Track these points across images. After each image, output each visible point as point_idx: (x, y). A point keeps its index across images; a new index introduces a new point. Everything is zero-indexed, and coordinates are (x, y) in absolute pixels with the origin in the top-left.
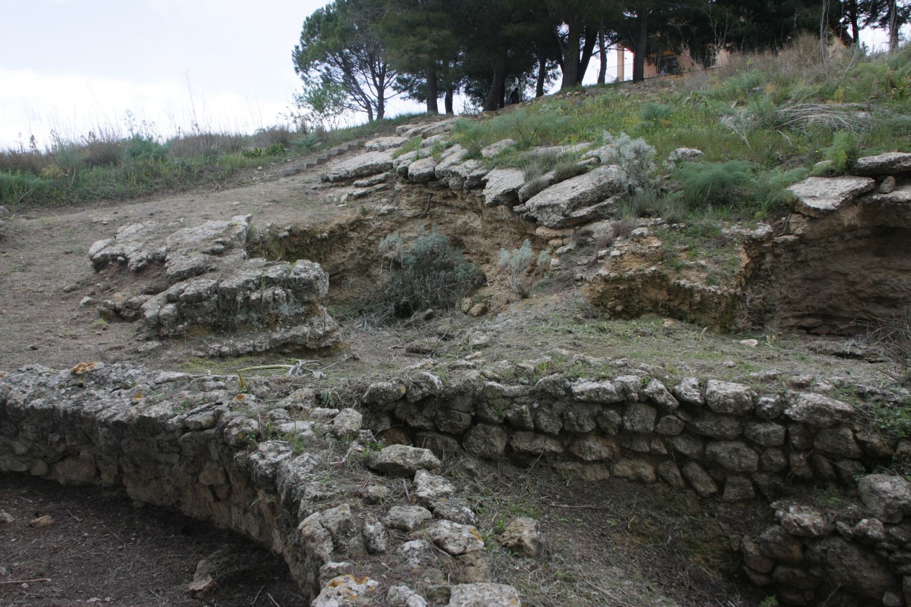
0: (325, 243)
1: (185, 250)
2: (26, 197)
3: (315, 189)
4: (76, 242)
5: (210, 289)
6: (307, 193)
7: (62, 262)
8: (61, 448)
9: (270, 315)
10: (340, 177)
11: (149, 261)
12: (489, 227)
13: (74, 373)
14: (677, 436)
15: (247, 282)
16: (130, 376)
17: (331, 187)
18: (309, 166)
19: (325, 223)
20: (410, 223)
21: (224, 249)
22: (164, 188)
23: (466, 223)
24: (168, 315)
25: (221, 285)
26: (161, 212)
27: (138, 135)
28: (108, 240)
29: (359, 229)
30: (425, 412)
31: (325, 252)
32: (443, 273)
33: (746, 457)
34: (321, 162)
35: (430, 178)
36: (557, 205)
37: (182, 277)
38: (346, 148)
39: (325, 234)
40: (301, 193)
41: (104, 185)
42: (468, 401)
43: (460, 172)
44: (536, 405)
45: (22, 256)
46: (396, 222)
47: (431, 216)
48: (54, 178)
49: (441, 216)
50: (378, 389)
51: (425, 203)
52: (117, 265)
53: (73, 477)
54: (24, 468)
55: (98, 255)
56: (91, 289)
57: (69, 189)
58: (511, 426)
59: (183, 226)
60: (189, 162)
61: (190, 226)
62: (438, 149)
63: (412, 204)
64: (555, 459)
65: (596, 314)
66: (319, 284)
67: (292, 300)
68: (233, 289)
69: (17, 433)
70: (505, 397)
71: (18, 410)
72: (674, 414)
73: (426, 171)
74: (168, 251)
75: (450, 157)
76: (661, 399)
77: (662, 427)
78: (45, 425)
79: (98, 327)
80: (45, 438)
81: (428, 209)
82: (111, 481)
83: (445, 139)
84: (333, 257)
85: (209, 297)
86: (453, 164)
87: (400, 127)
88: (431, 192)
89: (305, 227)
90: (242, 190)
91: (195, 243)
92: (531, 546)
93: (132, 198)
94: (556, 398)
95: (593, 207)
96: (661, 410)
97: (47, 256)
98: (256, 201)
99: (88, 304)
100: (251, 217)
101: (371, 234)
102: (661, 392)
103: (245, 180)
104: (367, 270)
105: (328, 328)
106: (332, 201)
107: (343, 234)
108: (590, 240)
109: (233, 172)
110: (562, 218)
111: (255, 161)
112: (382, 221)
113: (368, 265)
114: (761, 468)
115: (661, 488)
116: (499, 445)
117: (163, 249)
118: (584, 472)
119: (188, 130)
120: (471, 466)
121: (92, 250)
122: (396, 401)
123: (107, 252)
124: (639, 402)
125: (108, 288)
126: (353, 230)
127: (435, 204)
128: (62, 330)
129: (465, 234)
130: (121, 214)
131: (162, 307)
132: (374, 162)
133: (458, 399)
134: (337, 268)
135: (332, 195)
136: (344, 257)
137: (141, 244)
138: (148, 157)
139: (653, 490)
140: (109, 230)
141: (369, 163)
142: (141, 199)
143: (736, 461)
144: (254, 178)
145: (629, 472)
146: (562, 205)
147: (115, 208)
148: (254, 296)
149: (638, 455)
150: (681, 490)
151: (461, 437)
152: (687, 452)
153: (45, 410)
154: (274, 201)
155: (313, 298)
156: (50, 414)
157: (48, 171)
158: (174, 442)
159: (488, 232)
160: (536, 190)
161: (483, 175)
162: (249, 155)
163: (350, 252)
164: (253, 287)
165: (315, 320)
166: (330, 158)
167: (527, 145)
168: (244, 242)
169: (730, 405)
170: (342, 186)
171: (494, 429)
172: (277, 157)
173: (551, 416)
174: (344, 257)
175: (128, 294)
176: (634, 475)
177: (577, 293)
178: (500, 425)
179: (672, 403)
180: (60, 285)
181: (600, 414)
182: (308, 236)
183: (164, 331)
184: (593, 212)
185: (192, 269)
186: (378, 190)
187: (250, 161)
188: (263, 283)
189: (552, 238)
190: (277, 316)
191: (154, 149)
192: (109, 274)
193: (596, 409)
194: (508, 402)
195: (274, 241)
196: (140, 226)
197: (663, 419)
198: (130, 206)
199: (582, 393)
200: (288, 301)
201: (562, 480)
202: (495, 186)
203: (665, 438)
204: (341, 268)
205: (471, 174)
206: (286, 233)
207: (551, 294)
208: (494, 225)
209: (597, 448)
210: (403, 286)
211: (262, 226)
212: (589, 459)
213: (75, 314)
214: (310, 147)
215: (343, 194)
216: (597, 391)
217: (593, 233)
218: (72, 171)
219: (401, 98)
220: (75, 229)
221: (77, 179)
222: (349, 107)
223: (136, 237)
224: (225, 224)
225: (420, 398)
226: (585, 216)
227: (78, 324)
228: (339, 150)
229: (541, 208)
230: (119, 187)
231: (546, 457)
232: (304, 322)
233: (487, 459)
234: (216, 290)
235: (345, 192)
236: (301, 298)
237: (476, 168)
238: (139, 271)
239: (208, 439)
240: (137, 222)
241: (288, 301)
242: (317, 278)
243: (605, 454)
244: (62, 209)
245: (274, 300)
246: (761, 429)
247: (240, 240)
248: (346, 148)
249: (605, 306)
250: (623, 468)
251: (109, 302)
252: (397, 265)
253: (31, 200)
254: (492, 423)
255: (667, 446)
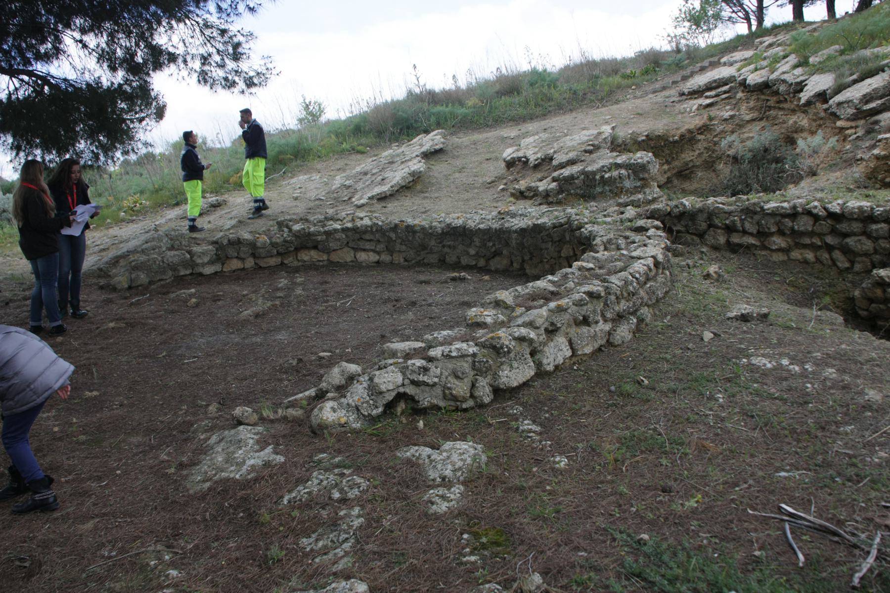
0: (676, 145)
1: (566, 151)
2: (456, 123)
3: (673, 102)
4: (493, 152)
5: (578, 172)
6: (666, 106)
7: (484, 166)
8: (493, 249)
9: (617, 187)
10: (694, 91)
11: (543, 160)
12: (814, 124)
13: (499, 213)
14: (827, 234)
15: (603, 167)
16: (529, 212)
17: (686, 99)
18: (674, 83)
19: (677, 129)
20: (749, 125)
21: (594, 150)
22: (555, 110)
23: (795, 122)
24: (553, 189)
25: (586, 169)
26: (552, 127)
27: (535, 68)
28: (515, 148)
29: (705, 133)
30: (682, 222)
31: (677, 152)
32: (774, 166)
33: (865, 244)
34: (685, 78)
35: (765, 87)
36: (851, 101)
37: (562, 166)
38: (707, 64)
39: (676, 138)
40: (661, 106)
41: (510, 110)
42: (705, 215)
43: (788, 79)
44: (743, 217)
45: (458, 163)
46: (737, 125)
47: (767, 118)
48: (474, 107)
49: (775, 118)
50: (654, 209)
51: (762, 107)
52: (521, 164)
53: (499, 267)
54: (474, 263)
55: (509, 158)
56: (505, 181)
57: (485, 115)
58: (730, 229)
59: (566, 135)
60: (575, 86)
61: (571, 135)
62: (776, 60)
63: (751, 109)
64: (756, 249)
65: (867, 185)
66: (650, 166)
67: (632, 178)
68: (594, 171)
69: (471, 244)
70: (725, 213)
71: (471, 230)
72: (824, 221)
73: (761, 80)
74: (555, 152)
75: (784, 67)
76: (815, 211)
77: (817, 229)
78: (485, 237)
79: (510, 202)
80: (485, 245)
81: (765, 113)
82: (518, 267)
83: (784, 51)
84: (683, 156)
85: (578, 177)
86: (784, 73)
87: (758, 40)
88: (767, 98)
89: (660, 132)
90: (615, 107)
91: (573, 146)
92: (714, 275)
93: (531, 119)
94: (755, 213)
95: (883, 100)
96: (816, 218)
97: (474, 162)
98: (624, 115)
99: (503, 190)
100: (616, 126)
101: (716, 136)
102: (816, 207)
103: (621, 98)
104: (712, 166)
105: (655, 196)
106: (686, 111)
107: (691, 137)
108: (877, 127)
109: (611, 93)
110: (855, 111)
111: (630, 81)
112: (725, 125)
113: (714, 162)
114: (876, 252)
115: (818, 266)
116: (722, 240)
117: (552, 151)
118: (771, 256)
119: (577, 59)
120: (704, 250)
121: (505, 155)
122: (665, 216)
123: (515, 155)
124: (803, 213)
125: (516, 180)
126: (701, 134)
127: (770, 108)
128: (488, 204)
129: (796, 132)
130: (524, 130)
131: (549, 184)
132: (721, 77)
133: (700, 215)
134: (687, 165)
135: (686, 106)
136: (693, 156)
137: (537, 149)
138: (543, 86)
139: (813, 268)
140: (515, 141)
141: (717, 77)
142: (539, 119)
143: (859, 247)
144: (628, 96)
145: (800, 257)
146: (855, 101)
147: (519, 127)
148: (607, 176)
149: (805, 246)
150: (829, 267)
151: (701, 235)
152: (832, 243)
153: (486, 229)
154: (638, 114)
155: (646, 175)
156: (488, 232)
157: (470, 103)
158: (549, 235)
159: (814, 129)
160: (839, 89)
161: (806, 80)
162: (625, 77)
163: (698, 152)
164: (607, 170)
165: (647, 191)
166: (692, 74)
167: (852, 48)
168: (609, 144)
169: (855, 213)
170: (696, 98)
171: (719, 231)
172: (649, 77)
173: (751, 223)
174: (693, 156)
175: (529, 181)
176: (802, 258)
177: (855, 169)
178: (723, 229)
179: (822, 213)
180: (484, 180)
181: (780, 221)
182: (662, 139)
183: (551, 199)
184: (882, 104)
185: (568, 161)
186: (723, 100)
187: (625, 82)
188: (613, 167)
189: (848, 129)
190: (622, 188)
191: (548, 79)
192: (517, 170)
193: (778, 218)
194: (727, 216)
195: (634, 144)
196: (537, 137)
197: (817, 224)
198: (529, 125)
199: (768, 209)
200: (629, 178)
201: (756, 260)
202: (811, 89)
203: (820, 235)
204: (691, 164)
205: (796, 81)
206: (644, 138)
207: (836, 172)
208: (818, 122)
209: (778, 241)
210: (740, 177)
211: (624, 133)
212: (774, 248)
213: (495, 196)
214: (679, 66)
215: (695, 104)
216: (777, 208)
217: (880, 121)
218: (487, 101)
219: (778, 6)
220: (492, 143)
221: (491, 107)
222: (728, 20)
223: (534, 144)
224: (595, 132)
225: (678, 213)
226: (874, 108)
227: (498, 201)
228: (701, 67)
229: (840, 104)
230: (521, 111)
231: (749, 247)
232: (640, 192)
233: (715, 248)
234: (583, 172)
235: (695, 103)
236: (638, 176)
237: (802, 75)
238: (536, 167)
239: (565, 231)
240: (533, 135)
241: (629, 178)
242: (649, 162)
243: (783, 245)
244: (482, 130)
245: (620, 177)
246: (874, 227)
247: (606, 143)
248: (707, 64)
249: (876, 178)
250: (796, 254)
251: (517, 187)
252: (735, 159)
253: (459, 125)
254: (718, 227)
255: (821, 240)
